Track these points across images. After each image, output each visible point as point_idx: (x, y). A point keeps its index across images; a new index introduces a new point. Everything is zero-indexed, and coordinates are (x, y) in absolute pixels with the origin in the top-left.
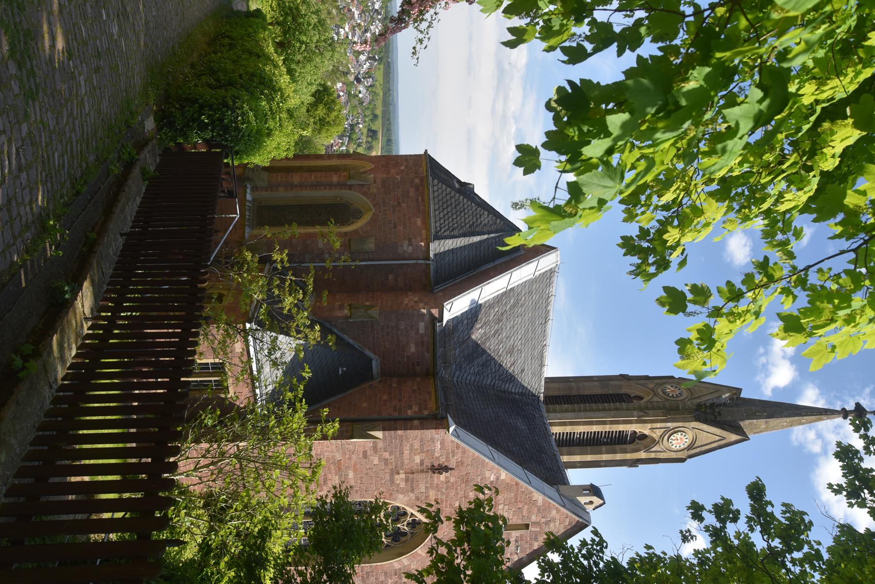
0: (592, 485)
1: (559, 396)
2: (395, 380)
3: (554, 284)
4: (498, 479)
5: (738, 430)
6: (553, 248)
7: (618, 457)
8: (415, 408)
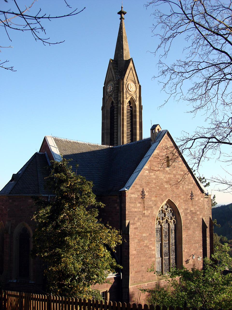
1: (110, 138)
3: (60, 138)
5: (128, 62)
7: (138, 114)
8: (116, 205)
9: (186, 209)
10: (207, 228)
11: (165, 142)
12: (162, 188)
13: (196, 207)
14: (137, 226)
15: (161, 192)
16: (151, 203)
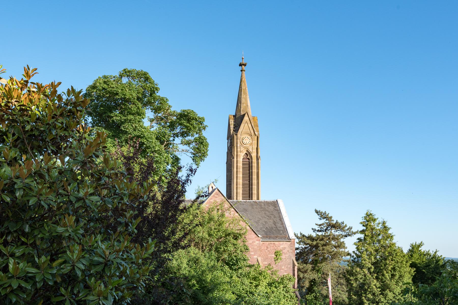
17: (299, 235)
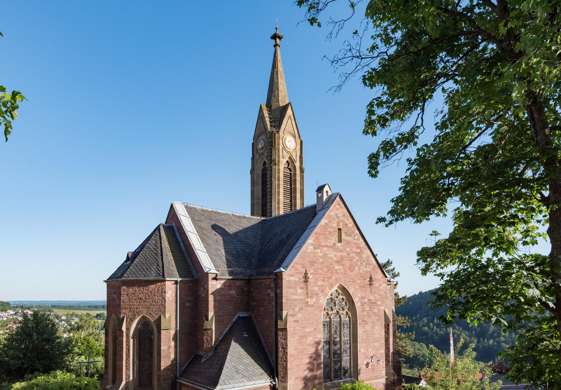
0: (317, 191)
2: (251, 303)
4: (312, 244)
5: (285, 108)
6: (172, 205)
8: (269, 291)
9: (363, 298)
10: (454, 273)
11: (336, 210)
12: (331, 269)
13: (376, 295)
14: (298, 319)
15: (329, 275)
16: (316, 289)
17: (423, 265)
